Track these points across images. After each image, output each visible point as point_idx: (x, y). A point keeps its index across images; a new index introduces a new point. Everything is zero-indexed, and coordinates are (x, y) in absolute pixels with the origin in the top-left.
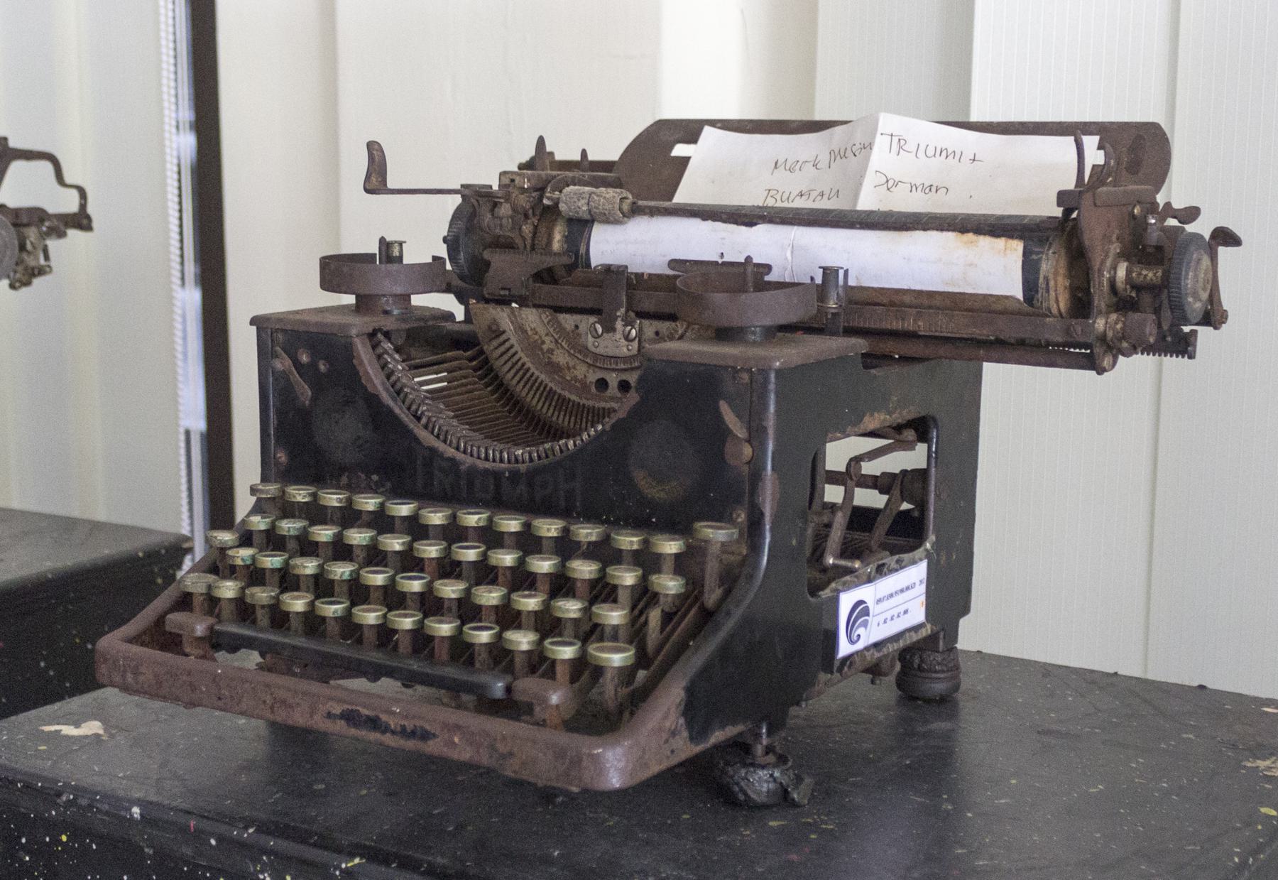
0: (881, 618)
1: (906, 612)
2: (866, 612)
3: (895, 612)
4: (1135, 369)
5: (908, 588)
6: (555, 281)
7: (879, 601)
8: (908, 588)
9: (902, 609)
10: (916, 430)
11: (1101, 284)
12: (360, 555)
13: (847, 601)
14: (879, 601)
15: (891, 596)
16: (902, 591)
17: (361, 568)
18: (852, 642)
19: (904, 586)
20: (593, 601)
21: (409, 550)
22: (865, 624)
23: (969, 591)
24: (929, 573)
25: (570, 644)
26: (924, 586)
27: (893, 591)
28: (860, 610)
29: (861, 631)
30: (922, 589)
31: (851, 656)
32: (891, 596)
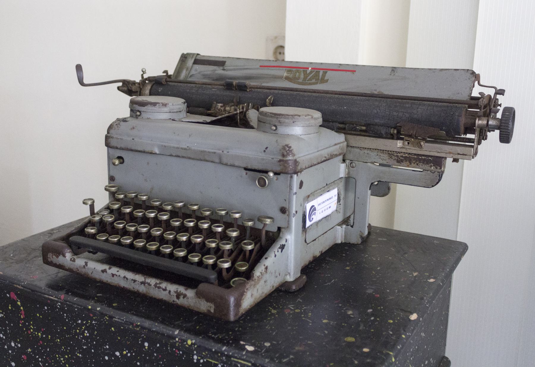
0: (321, 211)
1: (330, 207)
2: (315, 209)
3: (326, 208)
6: (126, 121)
7: (319, 204)
9: (328, 206)
11: (264, 82)
12: (190, 231)
14: (319, 204)
15: (324, 202)
17: (191, 235)
18: (310, 221)
21: (196, 225)
22: (315, 214)
23: (444, 239)
25: (236, 231)
28: (313, 209)
32: (324, 202)
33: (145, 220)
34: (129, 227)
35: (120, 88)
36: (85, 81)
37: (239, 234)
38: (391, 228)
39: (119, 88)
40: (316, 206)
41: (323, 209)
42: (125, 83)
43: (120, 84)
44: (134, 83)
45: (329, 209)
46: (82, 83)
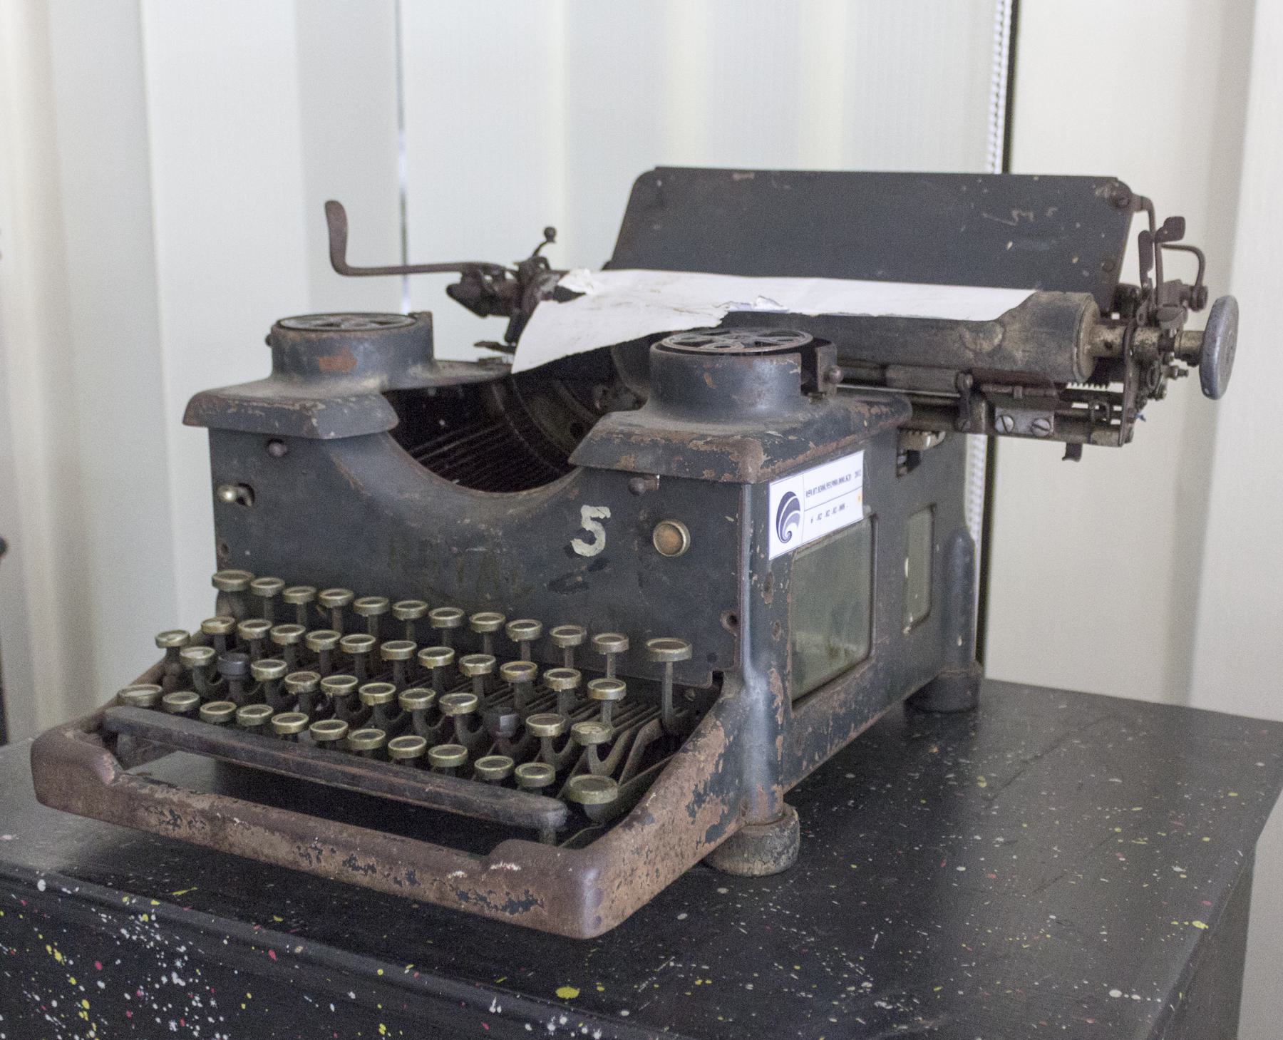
0: (814, 513)
1: (842, 507)
2: (795, 505)
3: (830, 506)
4: (268, 332)
5: (842, 480)
7: (809, 493)
8: (842, 480)
9: (837, 503)
10: (569, 819)
13: (777, 491)
14: (809, 493)
15: (823, 488)
16: (835, 483)
18: (784, 540)
19: (837, 477)
20: (382, 639)
22: (796, 520)
24: (864, 483)
26: (860, 478)
27: (825, 482)
29: (792, 527)
30: (858, 482)
31: (786, 558)
32: (823, 488)
33: (339, 662)
34: (247, 630)
35: (455, 293)
36: (352, 260)
37: (627, 647)
38: (1183, 704)
39: (451, 291)
40: (800, 496)
41: (823, 510)
42: (472, 272)
43: (455, 278)
44: (498, 272)
45: (839, 513)
46: (340, 266)
